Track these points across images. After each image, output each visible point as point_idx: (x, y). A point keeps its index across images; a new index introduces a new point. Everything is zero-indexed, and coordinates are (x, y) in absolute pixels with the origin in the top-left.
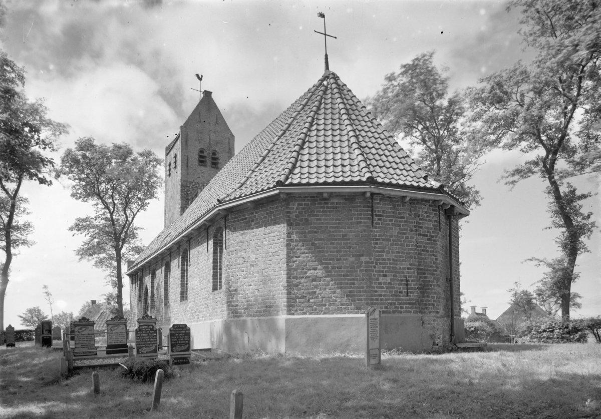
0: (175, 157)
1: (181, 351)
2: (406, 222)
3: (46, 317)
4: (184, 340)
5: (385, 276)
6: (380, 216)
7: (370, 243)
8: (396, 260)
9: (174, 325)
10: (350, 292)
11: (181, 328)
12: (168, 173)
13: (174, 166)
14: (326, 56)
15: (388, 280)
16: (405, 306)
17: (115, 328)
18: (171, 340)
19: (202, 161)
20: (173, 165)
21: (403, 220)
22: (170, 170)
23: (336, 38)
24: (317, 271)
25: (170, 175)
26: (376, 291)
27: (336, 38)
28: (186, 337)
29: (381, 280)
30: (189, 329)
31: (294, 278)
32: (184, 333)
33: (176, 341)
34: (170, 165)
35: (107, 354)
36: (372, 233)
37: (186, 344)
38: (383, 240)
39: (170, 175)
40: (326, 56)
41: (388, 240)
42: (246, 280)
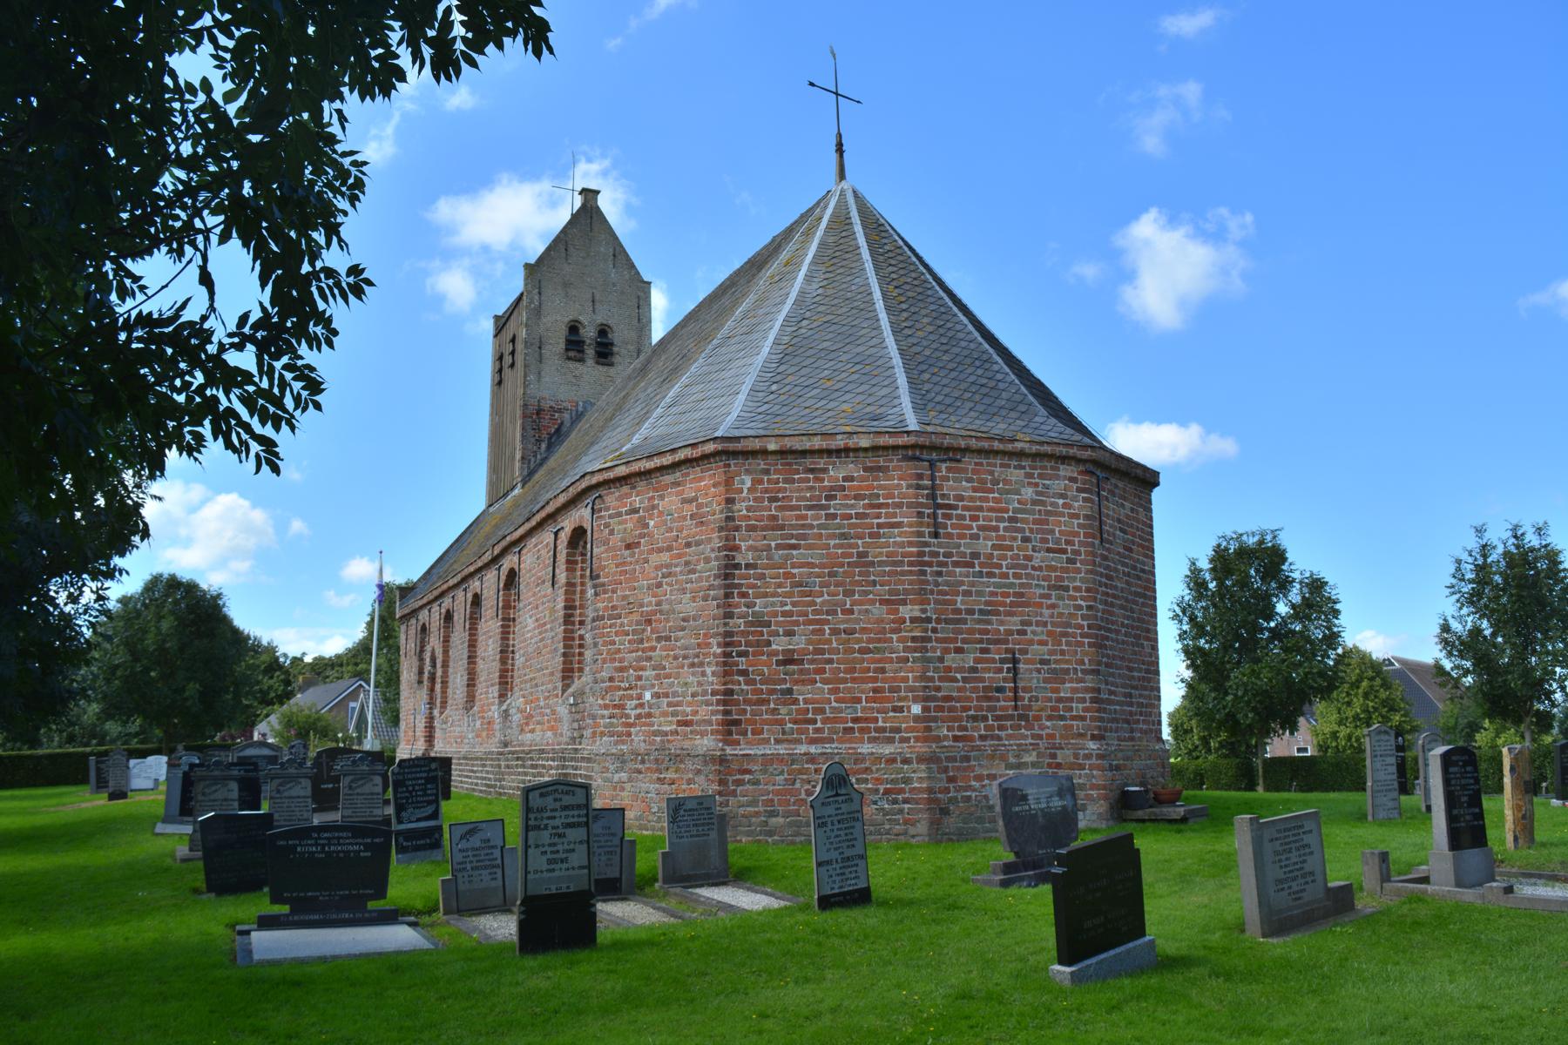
0: (513, 340)
1: (419, 820)
4: (425, 795)
8: (989, 613)
13: (511, 361)
14: (839, 135)
20: (508, 360)
22: (500, 371)
25: (500, 383)
26: (938, 689)
28: (429, 786)
32: (425, 778)
33: (407, 798)
37: (429, 803)
40: (839, 135)
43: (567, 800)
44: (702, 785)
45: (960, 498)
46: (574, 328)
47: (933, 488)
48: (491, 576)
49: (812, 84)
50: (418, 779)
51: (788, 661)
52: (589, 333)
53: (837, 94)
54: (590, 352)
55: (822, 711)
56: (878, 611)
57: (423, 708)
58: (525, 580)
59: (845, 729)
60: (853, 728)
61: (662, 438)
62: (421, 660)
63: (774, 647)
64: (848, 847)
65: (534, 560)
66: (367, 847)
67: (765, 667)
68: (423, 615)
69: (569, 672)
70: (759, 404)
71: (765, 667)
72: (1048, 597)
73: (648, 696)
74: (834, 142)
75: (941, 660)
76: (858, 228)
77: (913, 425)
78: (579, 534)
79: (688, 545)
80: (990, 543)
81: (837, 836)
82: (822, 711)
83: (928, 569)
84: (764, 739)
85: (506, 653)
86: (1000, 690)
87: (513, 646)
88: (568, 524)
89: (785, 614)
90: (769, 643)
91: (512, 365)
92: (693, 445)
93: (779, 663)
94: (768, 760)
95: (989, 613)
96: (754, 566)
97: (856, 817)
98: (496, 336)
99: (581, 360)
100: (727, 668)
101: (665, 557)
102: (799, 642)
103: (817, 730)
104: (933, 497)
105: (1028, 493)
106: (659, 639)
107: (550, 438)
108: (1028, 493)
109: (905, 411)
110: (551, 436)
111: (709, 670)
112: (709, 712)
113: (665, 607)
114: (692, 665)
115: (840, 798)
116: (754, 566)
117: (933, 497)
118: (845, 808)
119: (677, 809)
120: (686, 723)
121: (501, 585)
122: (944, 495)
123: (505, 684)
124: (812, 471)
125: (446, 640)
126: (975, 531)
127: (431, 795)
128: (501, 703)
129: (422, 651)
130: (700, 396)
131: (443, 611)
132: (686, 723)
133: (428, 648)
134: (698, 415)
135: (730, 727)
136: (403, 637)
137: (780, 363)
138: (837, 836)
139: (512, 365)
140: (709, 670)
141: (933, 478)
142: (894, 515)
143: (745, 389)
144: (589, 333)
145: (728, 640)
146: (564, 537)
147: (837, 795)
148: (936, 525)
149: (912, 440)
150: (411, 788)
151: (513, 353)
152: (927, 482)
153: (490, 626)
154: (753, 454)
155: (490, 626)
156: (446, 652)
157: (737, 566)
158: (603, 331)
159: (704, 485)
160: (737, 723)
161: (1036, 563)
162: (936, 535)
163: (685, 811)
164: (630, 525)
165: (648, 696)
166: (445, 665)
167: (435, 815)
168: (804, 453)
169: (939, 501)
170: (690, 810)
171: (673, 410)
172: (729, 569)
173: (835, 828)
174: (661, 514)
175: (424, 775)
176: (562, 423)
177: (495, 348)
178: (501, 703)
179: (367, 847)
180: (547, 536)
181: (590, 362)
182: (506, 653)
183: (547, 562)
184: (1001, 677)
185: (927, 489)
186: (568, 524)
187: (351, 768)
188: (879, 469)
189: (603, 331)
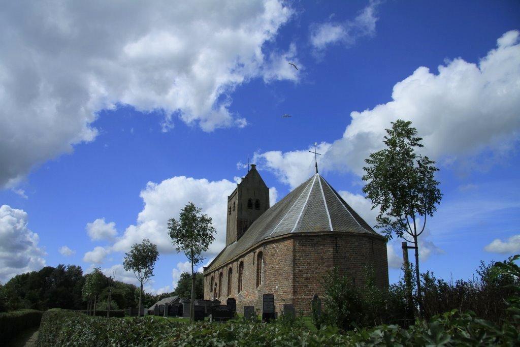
0: (234, 204)
14: (316, 163)
20: (232, 209)
22: (230, 211)
25: (230, 214)
34: (230, 208)
40: (316, 163)
43: (270, 297)
44: (290, 303)
45: (342, 245)
46: (250, 200)
47: (336, 243)
48: (235, 264)
52: (254, 202)
54: (254, 206)
55: (313, 289)
56: (325, 268)
58: (246, 265)
61: (279, 232)
65: (248, 259)
66: (228, 309)
67: (302, 280)
68: (212, 274)
69: (258, 284)
71: (302, 280)
72: (361, 265)
73: (277, 287)
76: (321, 185)
77: (332, 230)
79: (285, 255)
82: (313, 289)
85: (240, 281)
88: (257, 251)
89: (306, 269)
91: (234, 210)
92: (286, 234)
93: (305, 279)
94: (303, 299)
96: (299, 260)
98: (228, 202)
99: (252, 209)
100: (294, 280)
101: (281, 258)
102: (309, 275)
104: (336, 245)
105: (357, 244)
106: (279, 275)
108: (357, 244)
110: (244, 228)
111: (290, 281)
112: (290, 290)
113: (281, 268)
114: (286, 280)
116: (299, 260)
117: (336, 245)
119: (286, 306)
120: (285, 292)
123: (240, 289)
124: (311, 240)
128: (238, 293)
132: (285, 292)
134: (287, 227)
135: (295, 293)
136: (205, 281)
137: (304, 216)
139: (234, 210)
140: (290, 281)
143: (297, 222)
144: (254, 202)
145: (294, 275)
146: (256, 254)
149: (332, 233)
151: (234, 207)
152: (335, 242)
154: (299, 236)
156: (220, 283)
157: (296, 260)
158: (257, 201)
159: (289, 243)
160: (296, 292)
161: (359, 258)
162: (337, 253)
164: (273, 251)
165: (277, 287)
168: (310, 236)
171: (282, 226)
172: (294, 260)
174: (279, 248)
177: (228, 205)
178: (238, 293)
179: (228, 309)
180: (252, 254)
181: (254, 209)
182: (240, 281)
183: (251, 257)
186: (257, 251)
188: (325, 239)
189: (257, 201)
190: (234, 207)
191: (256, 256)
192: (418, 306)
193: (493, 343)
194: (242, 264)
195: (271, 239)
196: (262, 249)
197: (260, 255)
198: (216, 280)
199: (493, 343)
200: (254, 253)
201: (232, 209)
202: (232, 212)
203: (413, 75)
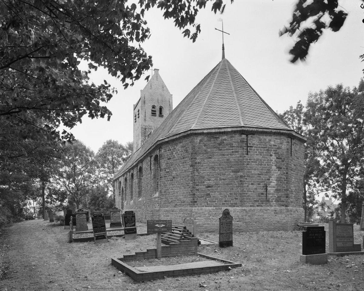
0: (139, 111)
1: (130, 226)
2: (267, 150)
3: (300, 106)
4: (132, 220)
5: (252, 184)
6: (251, 147)
7: (244, 164)
8: (260, 174)
9: (126, 212)
10: (230, 194)
11: (130, 213)
12: (135, 121)
13: (138, 116)
14: (223, 45)
15: (255, 187)
16: (265, 202)
17: (80, 216)
18: (124, 220)
19: (154, 113)
20: (137, 116)
21: (266, 149)
22: (136, 119)
23: (229, 34)
24: (211, 181)
25: (136, 122)
26: (247, 194)
27: (229, 34)
28: (133, 218)
29: (250, 186)
30: (135, 214)
31: (197, 185)
32: (132, 216)
33: (127, 221)
34: (136, 116)
35: (323, 227)
36: (245, 158)
37: (133, 222)
38: (252, 162)
39: (136, 122)
40: (223, 45)
41: (255, 162)
42: (170, 186)
46: (154, 107)
49: (216, 29)
50: (130, 216)
51: (209, 187)
53: (223, 32)
55: (217, 199)
57: (121, 201)
59: (223, 203)
60: (224, 203)
62: (120, 189)
63: (205, 183)
64: (228, 230)
67: (202, 187)
70: (202, 121)
71: (202, 187)
74: (222, 47)
75: (248, 186)
78: (156, 156)
80: (261, 156)
81: (225, 227)
83: (245, 163)
84: (202, 206)
86: (262, 194)
87: (141, 185)
90: (204, 182)
91: (139, 117)
95: (260, 174)
97: (231, 223)
102: (212, 183)
103: (216, 204)
107: (148, 136)
109: (241, 121)
115: (227, 218)
118: (228, 220)
121: (138, 171)
122: (250, 143)
125: (126, 185)
126: (258, 153)
127: (134, 220)
129: (120, 187)
130: (186, 120)
131: (125, 178)
133: (121, 187)
138: (225, 227)
139: (139, 117)
141: (247, 139)
142: (237, 149)
147: (226, 217)
148: (247, 152)
150: (128, 219)
151: (139, 114)
153: (136, 180)
155: (136, 180)
160: (196, 202)
162: (247, 154)
163: (187, 220)
166: (125, 190)
167: (134, 225)
169: (248, 145)
170: (188, 220)
173: (225, 225)
175: (132, 215)
176: (151, 132)
182: (140, 187)
184: (262, 191)
185: (245, 142)
187: (78, 213)
190: (139, 114)
191: (153, 159)
192: (66, 16)
193: (135, 80)
194: (141, 170)
195: (167, 140)
196: (157, 152)
197: (156, 158)
198: (123, 185)
199: (135, 80)
200: (151, 157)
201: (137, 116)
202: (137, 119)
203: (335, 32)
